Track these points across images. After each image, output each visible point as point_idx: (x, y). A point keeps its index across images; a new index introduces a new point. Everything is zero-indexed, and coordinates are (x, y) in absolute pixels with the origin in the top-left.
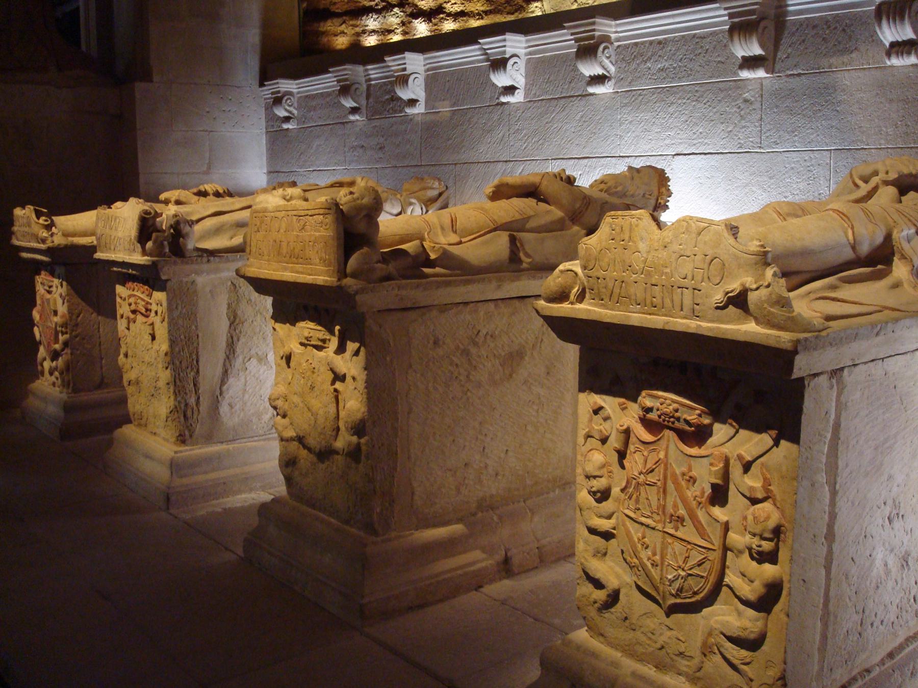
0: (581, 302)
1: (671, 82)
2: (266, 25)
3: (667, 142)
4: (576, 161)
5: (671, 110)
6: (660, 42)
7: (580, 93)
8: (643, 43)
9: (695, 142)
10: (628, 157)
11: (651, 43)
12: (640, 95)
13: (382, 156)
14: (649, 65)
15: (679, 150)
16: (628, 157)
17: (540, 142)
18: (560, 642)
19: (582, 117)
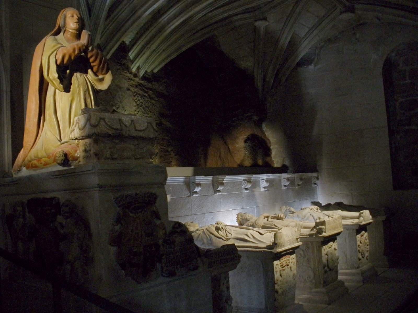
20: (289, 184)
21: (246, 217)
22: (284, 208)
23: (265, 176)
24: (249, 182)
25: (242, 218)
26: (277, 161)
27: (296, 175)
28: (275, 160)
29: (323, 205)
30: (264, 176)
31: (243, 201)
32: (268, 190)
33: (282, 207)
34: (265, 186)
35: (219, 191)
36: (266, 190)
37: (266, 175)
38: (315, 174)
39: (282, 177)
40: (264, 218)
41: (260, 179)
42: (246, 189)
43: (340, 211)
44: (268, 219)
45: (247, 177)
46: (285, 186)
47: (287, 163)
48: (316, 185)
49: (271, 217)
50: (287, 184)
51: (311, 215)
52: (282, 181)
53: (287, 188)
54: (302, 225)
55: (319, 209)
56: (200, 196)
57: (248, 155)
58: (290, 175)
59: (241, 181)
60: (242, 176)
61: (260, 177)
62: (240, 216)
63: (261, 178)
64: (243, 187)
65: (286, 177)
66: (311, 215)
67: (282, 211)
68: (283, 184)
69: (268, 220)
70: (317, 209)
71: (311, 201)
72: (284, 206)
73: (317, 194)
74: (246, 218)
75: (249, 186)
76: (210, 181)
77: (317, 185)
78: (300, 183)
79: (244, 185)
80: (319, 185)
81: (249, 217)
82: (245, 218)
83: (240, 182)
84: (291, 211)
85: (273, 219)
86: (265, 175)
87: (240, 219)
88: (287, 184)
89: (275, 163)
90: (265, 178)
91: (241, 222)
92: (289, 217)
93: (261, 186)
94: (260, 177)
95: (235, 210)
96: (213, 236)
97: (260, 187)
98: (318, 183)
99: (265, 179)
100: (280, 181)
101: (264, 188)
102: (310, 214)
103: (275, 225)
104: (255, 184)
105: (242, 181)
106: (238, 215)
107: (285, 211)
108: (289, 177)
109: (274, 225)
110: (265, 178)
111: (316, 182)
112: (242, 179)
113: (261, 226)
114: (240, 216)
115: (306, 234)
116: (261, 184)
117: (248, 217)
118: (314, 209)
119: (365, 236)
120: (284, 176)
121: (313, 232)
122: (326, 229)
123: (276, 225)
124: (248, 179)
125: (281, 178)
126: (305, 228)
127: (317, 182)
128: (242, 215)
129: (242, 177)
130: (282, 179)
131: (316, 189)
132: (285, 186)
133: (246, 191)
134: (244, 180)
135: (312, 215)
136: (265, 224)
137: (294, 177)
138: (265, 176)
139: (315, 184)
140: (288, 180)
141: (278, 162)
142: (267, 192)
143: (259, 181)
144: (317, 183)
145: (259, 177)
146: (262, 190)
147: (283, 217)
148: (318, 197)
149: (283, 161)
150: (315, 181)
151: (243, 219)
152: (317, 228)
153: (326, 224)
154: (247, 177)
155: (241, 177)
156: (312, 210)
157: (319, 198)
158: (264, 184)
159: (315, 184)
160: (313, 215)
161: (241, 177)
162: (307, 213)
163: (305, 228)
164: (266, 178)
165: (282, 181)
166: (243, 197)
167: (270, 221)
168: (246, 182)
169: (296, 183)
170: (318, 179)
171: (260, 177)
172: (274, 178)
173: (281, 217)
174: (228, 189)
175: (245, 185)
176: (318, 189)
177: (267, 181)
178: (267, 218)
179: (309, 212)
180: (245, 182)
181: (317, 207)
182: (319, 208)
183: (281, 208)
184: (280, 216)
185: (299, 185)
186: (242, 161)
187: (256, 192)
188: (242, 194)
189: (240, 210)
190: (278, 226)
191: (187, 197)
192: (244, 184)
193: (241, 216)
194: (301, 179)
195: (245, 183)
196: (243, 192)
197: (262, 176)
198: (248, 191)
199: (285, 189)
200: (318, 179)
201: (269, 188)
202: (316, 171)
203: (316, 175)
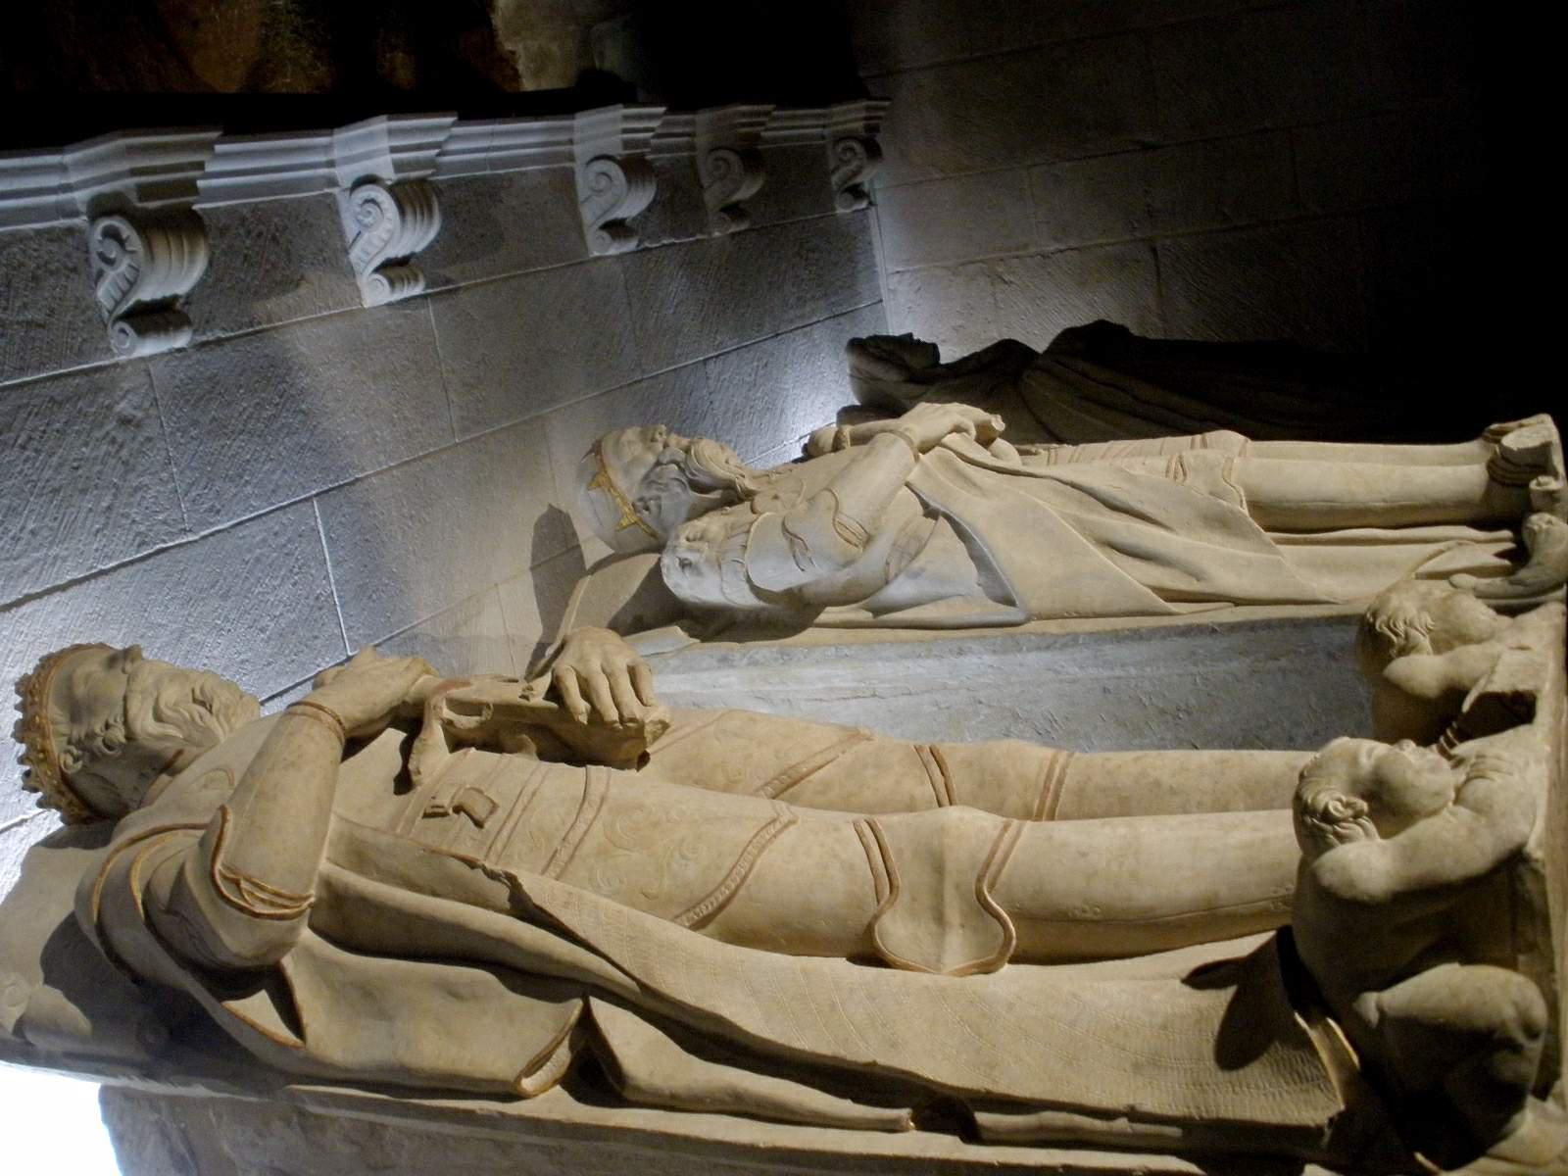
9: (24, 562)
20: (649, 209)
21: (126, 723)
22: (633, 455)
23: (386, 143)
24: (169, 219)
25: (79, 732)
26: (534, 54)
27: (703, 121)
28: (520, 49)
29: (948, 355)
30: (373, 147)
31: (128, 467)
32: (443, 291)
33: (608, 447)
34: (398, 251)
36: (418, 290)
37: (391, 133)
38: (849, 116)
39: (577, 149)
40: (354, 744)
41: (332, 182)
42: (153, 317)
43: (1229, 440)
44: (406, 749)
45: (126, 165)
46: (616, 228)
47: (612, 58)
48: (864, 205)
49: (448, 725)
50: (634, 204)
51: (931, 513)
52: (585, 180)
53: (631, 245)
54: (987, 870)
55: (1004, 436)
56: (204, 344)
57: (298, 21)
58: (651, 117)
59: (70, 231)
60: (63, 169)
61: (331, 164)
62: (54, 713)
63: (346, 174)
64: (104, 294)
65: (614, 145)
66: (931, 513)
67: (611, 486)
68: (591, 215)
69: (404, 782)
70: (985, 439)
71: (845, 342)
72: (631, 434)
73: (871, 267)
74: (130, 737)
75: (177, 275)
77: (871, 204)
78: (747, 191)
79: (111, 274)
80: (879, 198)
81: (158, 717)
82: (118, 734)
83: (51, 236)
84: (702, 479)
85: (491, 741)
86: (380, 124)
87: (56, 745)
88: (634, 204)
89: (521, 68)
90: (384, 167)
91: (84, 784)
92: (692, 557)
93: (355, 255)
94: (336, 154)
95: (26, 609)
97: (349, 273)
98: (877, 186)
99: (389, 175)
100: (564, 183)
101: (394, 268)
102: (925, 505)
103: (512, 881)
104: (279, 247)
105: (81, 221)
106: (29, 690)
107: (648, 480)
108: (645, 143)
109: (502, 893)
110: (384, 167)
111: (858, 180)
112: (81, 196)
113: (313, 893)
114: (54, 713)
115: (1133, 1115)
116: (350, 237)
117: (145, 724)
118: (952, 439)
120: (602, 129)
121: (1265, 1098)
123: (539, 888)
124: (145, 192)
125: (571, 158)
126: (1065, 933)
127: (864, 179)
128: (80, 690)
129: (73, 178)
130: (578, 166)
131: (865, 229)
132: (616, 228)
133: (151, 347)
134: (100, 208)
135: (948, 518)
136: (359, 856)
137: (692, 147)
138: (386, 143)
139: (857, 192)
140: (635, 167)
141: (542, 60)
142: (429, 312)
143: (331, 207)
144: (866, 188)
145: (322, 158)
146: (376, 293)
147: (633, 707)
148: (883, 291)
149: (585, 43)
150: (855, 174)
151: (84, 746)
152: (1372, 1003)
153: (1541, 919)
154: (126, 165)
155: (53, 181)
156: (937, 448)
157: (889, 304)
158: (381, 233)
159: (857, 192)
160: (956, 510)
161: (53, 181)
162: (892, 494)
163: (1065, 933)
164: (399, 166)
165: (582, 191)
166: (125, 421)
167: (445, 801)
168: (126, 230)
169: (712, 197)
170: (873, 151)
171: (336, 154)
172: (493, 164)
173: (595, 713)
175: (123, 266)
176: (874, 230)
177: (412, 195)
178: (394, 737)
179: (907, 485)
180: (112, 234)
181: (979, 414)
182: (998, 423)
183: (597, 449)
184: (581, 706)
185: (734, 211)
186: (259, 70)
187: (305, 330)
188: (99, 381)
189: (101, 583)
190: (567, 918)
192: (110, 262)
193: (76, 710)
194: (752, 156)
195: (113, 251)
196: (123, 358)
197: (347, 143)
198: (182, 340)
199: (621, 257)
200: (873, 151)
201: (450, 272)
202: (854, 91)
203: (859, 125)
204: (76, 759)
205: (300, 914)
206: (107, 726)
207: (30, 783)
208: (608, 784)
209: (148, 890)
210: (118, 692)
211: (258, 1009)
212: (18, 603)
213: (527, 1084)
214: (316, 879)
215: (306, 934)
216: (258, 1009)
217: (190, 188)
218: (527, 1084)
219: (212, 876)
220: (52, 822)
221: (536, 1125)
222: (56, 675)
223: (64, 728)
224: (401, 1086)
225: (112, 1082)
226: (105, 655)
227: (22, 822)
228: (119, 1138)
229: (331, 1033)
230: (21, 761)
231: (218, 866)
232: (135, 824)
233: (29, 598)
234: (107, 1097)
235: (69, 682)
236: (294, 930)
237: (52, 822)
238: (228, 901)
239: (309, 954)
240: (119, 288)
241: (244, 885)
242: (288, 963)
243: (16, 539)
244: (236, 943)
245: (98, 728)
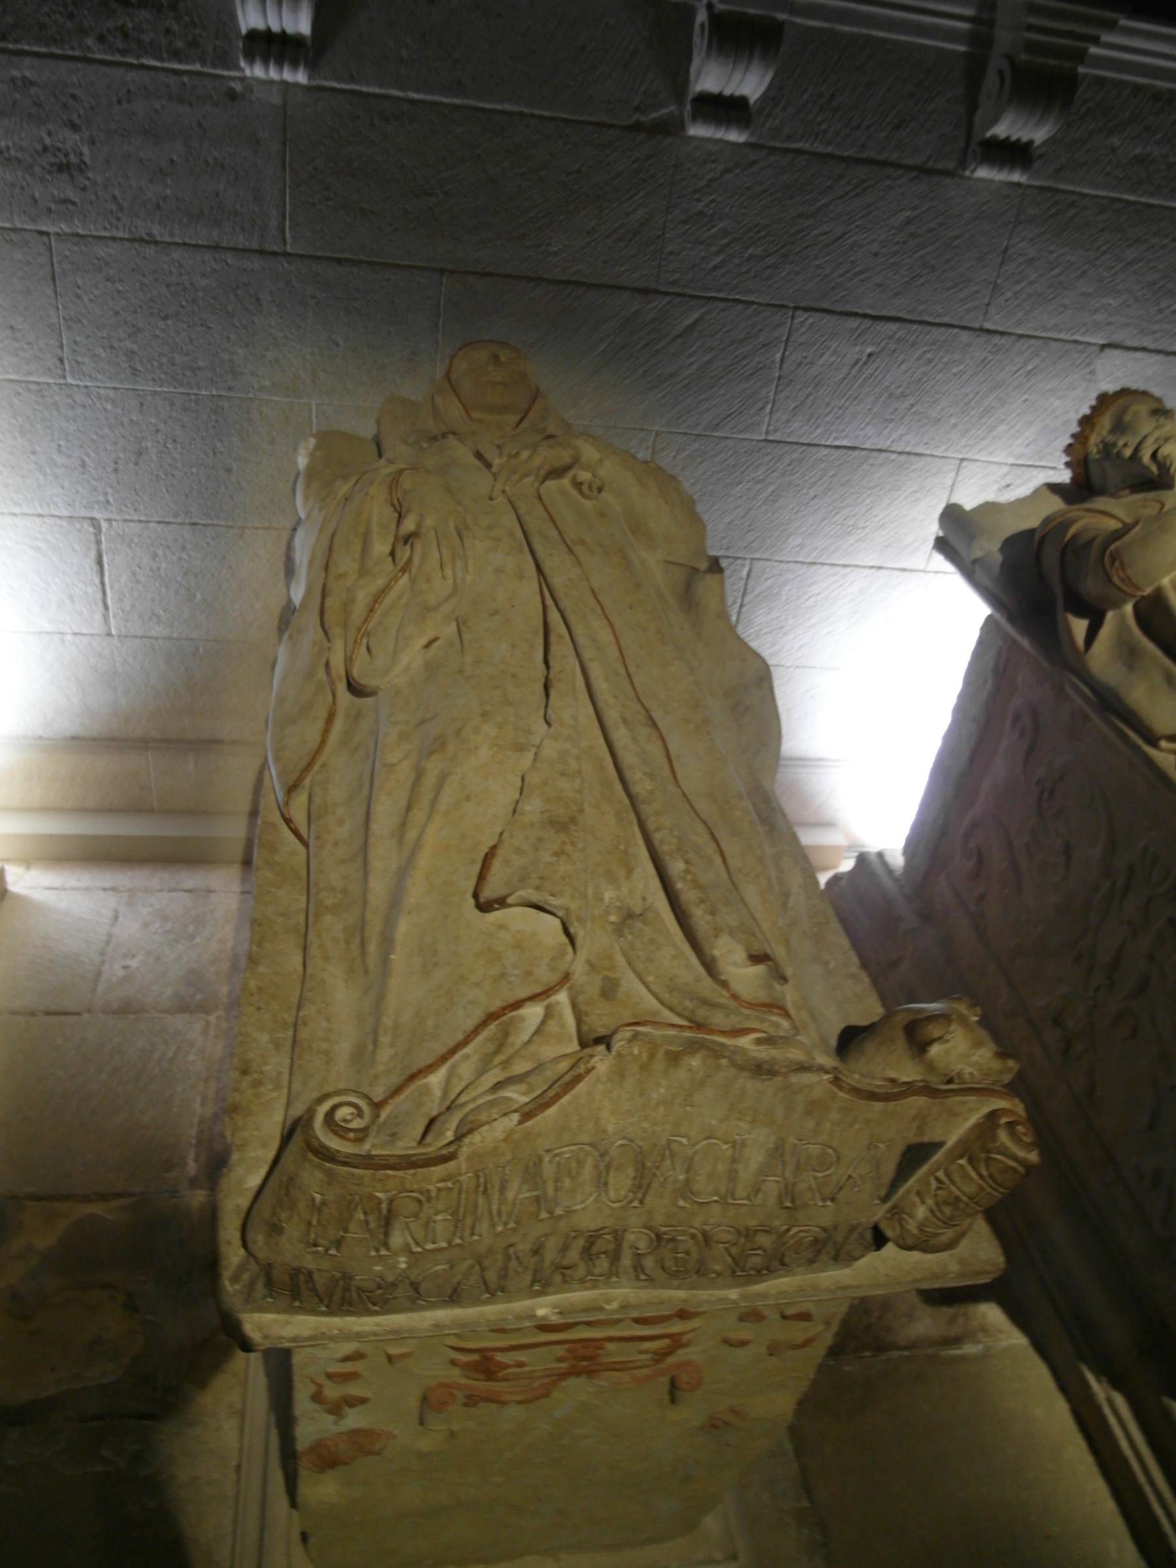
0: (862, 1331)
1: (1152, 195)
2: (684, 1333)
3: (1098, 317)
4: (867, 323)
5: (1130, 254)
6: (1157, 95)
7: (917, 160)
8: (1117, 84)
9: (1156, 327)
10: (1002, 334)
11: (1138, 89)
12: (1072, 204)
13: (71, 194)
14: (1115, 140)
15: (1118, 337)
16: (1002, 334)
17: (771, 260)
18: (148, 40)
19: (909, 222)
35: (1013, 153)
76: (950, 35)
87: (1094, 439)
91: (1094, 469)
95: (1139, 355)
96: (241, 241)
113: (1148, 591)
119: (197, 1105)
122: (251, 944)
128: (1127, 418)
151: (1107, 449)
174: (1140, 160)
191: (637, 127)
193: (1119, 427)
204: (1098, 452)
205: (1133, 596)
206: (1125, 445)
207: (1069, 449)
208: (629, 675)
209: (1075, 537)
210: (1145, 430)
211: (1079, 626)
212: (1136, 349)
213: (1164, 744)
214: (1156, 585)
215: (1129, 608)
216: (1079, 626)
217: (1080, 56)
218: (1164, 744)
219: (1105, 550)
220: (1064, 476)
221: (1150, 762)
222: (1121, 402)
223: (1105, 432)
224: (1110, 704)
225: (998, 616)
226: (1154, 405)
227: (1054, 468)
228: (981, 642)
229: (1102, 657)
230: (1073, 436)
231: (1113, 547)
232: (1101, 503)
233: (1143, 349)
234: (989, 619)
235: (1124, 411)
236: (1124, 602)
237: (1064, 476)
238: (1103, 566)
239: (1123, 619)
240: (742, 80)
241: (1117, 564)
242: (1110, 615)
243: (1160, 311)
244: (1090, 587)
245: (1121, 443)
